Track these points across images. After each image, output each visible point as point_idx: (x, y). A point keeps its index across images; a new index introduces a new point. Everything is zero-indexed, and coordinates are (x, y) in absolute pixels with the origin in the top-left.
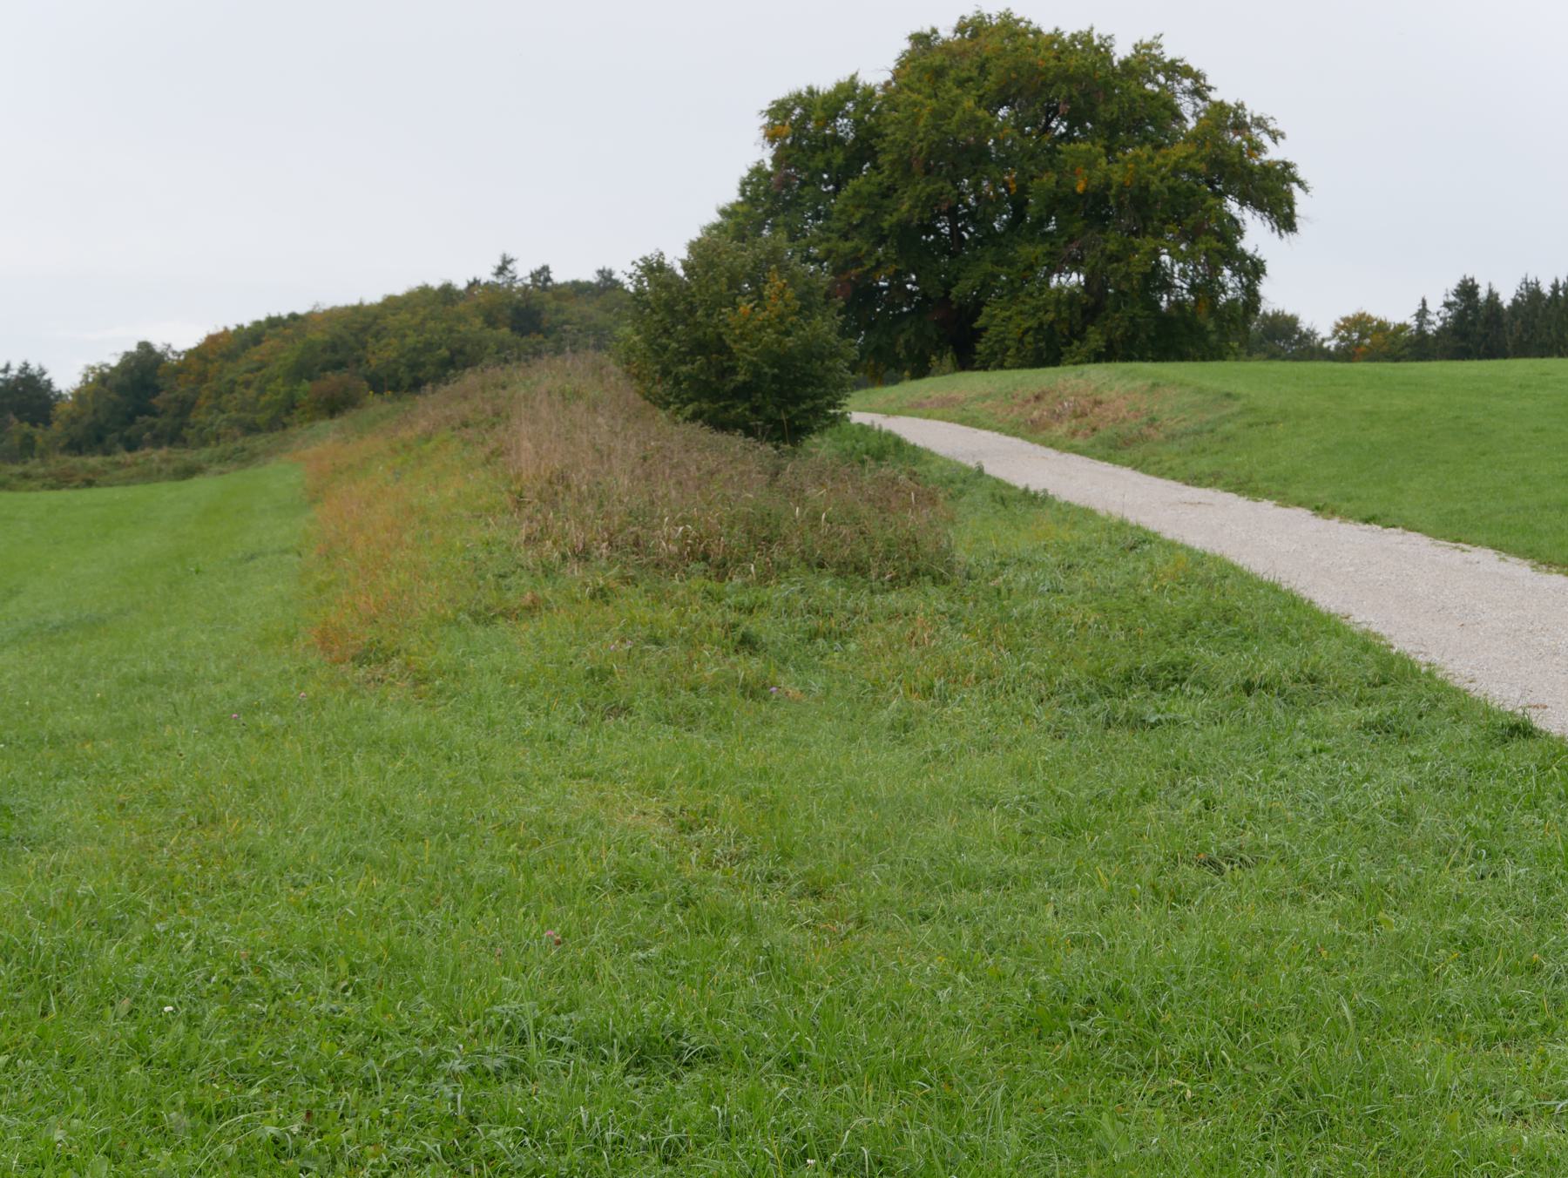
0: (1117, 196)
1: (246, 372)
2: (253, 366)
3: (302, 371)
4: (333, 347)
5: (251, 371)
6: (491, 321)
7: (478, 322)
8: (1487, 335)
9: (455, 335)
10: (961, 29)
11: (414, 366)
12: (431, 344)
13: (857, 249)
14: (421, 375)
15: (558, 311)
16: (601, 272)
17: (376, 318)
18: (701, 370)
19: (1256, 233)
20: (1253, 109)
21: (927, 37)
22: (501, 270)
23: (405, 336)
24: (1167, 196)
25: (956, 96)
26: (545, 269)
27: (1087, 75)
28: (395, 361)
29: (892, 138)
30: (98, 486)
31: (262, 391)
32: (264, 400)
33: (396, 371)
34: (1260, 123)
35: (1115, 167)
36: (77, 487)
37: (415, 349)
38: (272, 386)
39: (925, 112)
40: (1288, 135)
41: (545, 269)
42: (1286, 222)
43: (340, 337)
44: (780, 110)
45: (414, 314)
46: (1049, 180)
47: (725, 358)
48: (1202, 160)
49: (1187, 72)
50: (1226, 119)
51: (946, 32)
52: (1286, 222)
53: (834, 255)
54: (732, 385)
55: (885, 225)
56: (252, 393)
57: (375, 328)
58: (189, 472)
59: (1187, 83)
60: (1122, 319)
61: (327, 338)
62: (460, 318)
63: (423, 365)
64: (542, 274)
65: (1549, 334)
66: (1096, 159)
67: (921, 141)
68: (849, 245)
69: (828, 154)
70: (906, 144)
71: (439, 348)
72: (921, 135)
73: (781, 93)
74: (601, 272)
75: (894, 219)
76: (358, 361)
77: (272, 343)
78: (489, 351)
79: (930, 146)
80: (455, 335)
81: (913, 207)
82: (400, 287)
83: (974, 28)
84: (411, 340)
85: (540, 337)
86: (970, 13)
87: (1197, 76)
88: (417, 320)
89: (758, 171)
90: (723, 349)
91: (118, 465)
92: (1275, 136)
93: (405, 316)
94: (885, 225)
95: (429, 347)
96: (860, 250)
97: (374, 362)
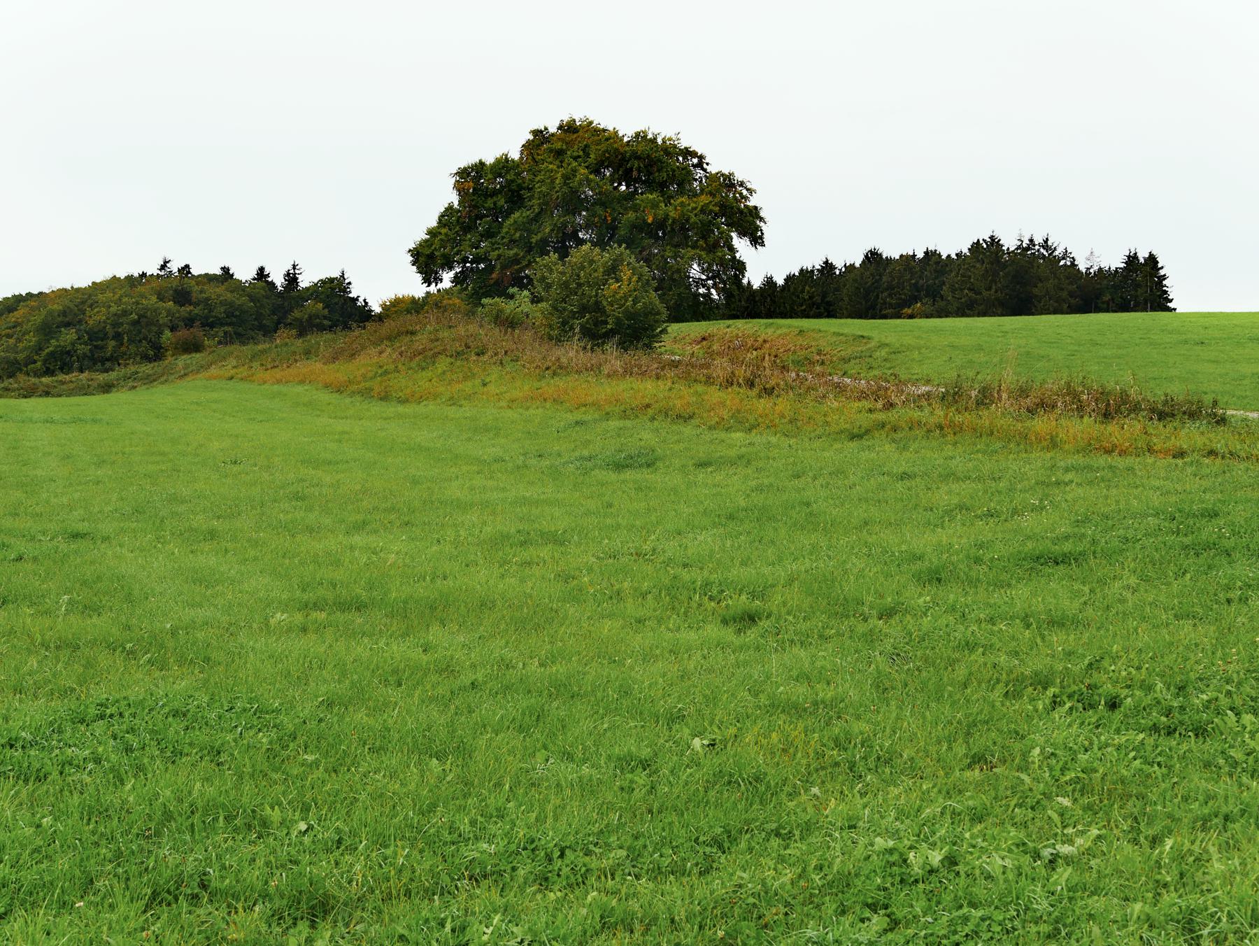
0: (671, 225)
1: (7, 328)
2: (11, 324)
3: (48, 330)
4: (64, 313)
5: (10, 328)
6: (161, 298)
7: (154, 299)
8: (748, 307)
9: (140, 306)
10: (560, 128)
11: (115, 325)
12: (126, 311)
13: (516, 254)
14: (120, 330)
15: (201, 292)
16: (222, 268)
17: (90, 296)
18: (587, 322)
19: (742, 246)
20: (739, 176)
21: (541, 132)
22: (163, 267)
23: (110, 307)
24: (700, 225)
25: (575, 167)
26: (187, 266)
27: (648, 156)
28: (104, 322)
29: (539, 190)
30: (53, 396)
31: (18, 340)
32: (21, 345)
33: (105, 327)
34: (742, 184)
35: (671, 208)
36: (40, 396)
37: (115, 315)
38: (27, 337)
39: (559, 175)
40: (757, 192)
41: (187, 266)
42: (757, 240)
43: (69, 307)
44: (463, 173)
45: (115, 293)
46: (631, 215)
47: (599, 315)
48: (715, 205)
49: (694, 154)
50: (727, 182)
51: (553, 129)
52: (757, 240)
53: (502, 258)
54: (604, 330)
55: (533, 240)
56: (12, 341)
57: (90, 302)
58: (107, 388)
59: (695, 161)
60: (674, 295)
61: (61, 308)
62: (143, 296)
63: (122, 324)
64: (186, 269)
65: (785, 307)
66: (658, 203)
67: (557, 192)
68: (512, 252)
69: (495, 199)
70: (548, 194)
71: (131, 314)
72: (557, 189)
73: (463, 164)
74: (222, 268)
75: (539, 236)
76: (80, 322)
77: (23, 311)
78: (161, 316)
79: (563, 195)
80: (140, 306)
81: (552, 230)
82: (101, 274)
83: (640, 137)
84: (114, 309)
85: (192, 308)
86: (566, 119)
87: (701, 158)
88: (117, 297)
89: (450, 208)
90: (603, 311)
91: (62, 383)
92: (750, 191)
93: (109, 294)
94: (533, 240)
95: (125, 313)
96: (519, 255)
97: (91, 322)
